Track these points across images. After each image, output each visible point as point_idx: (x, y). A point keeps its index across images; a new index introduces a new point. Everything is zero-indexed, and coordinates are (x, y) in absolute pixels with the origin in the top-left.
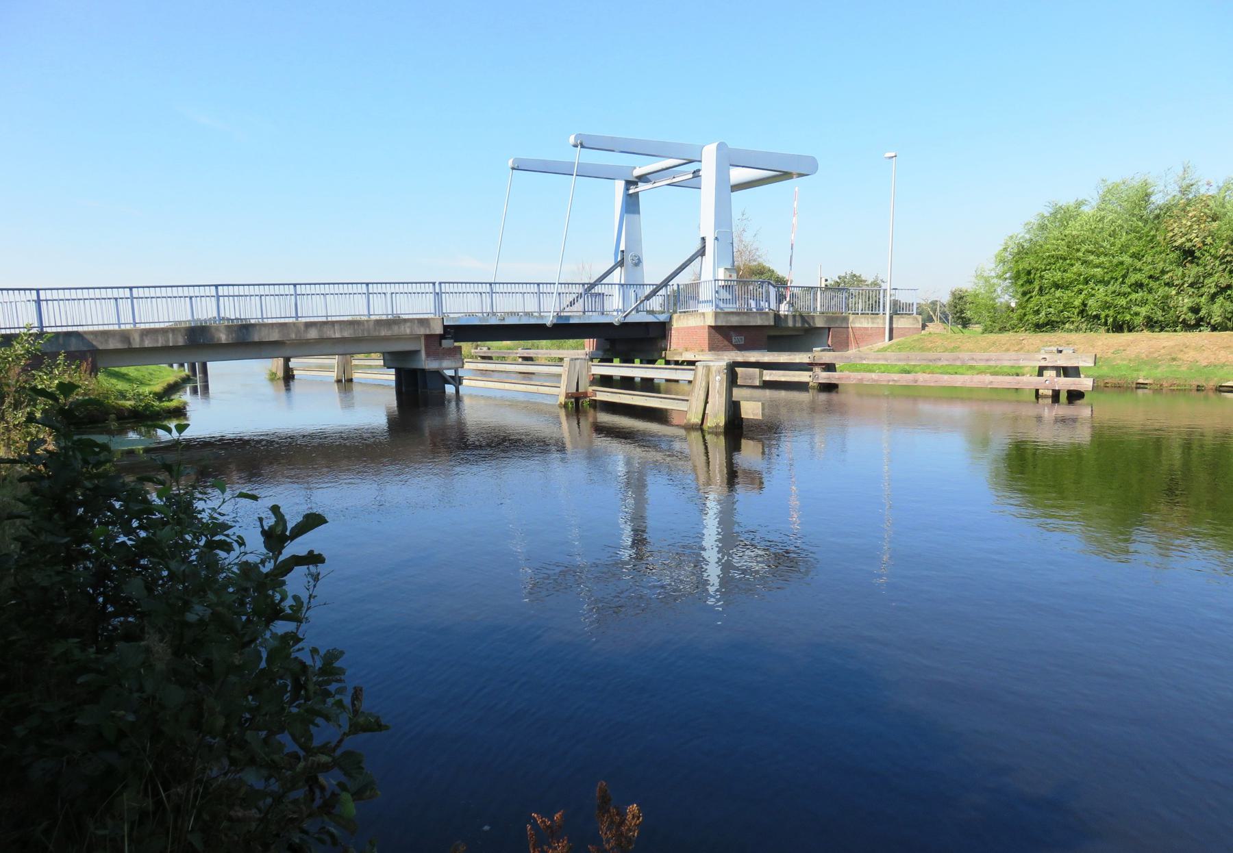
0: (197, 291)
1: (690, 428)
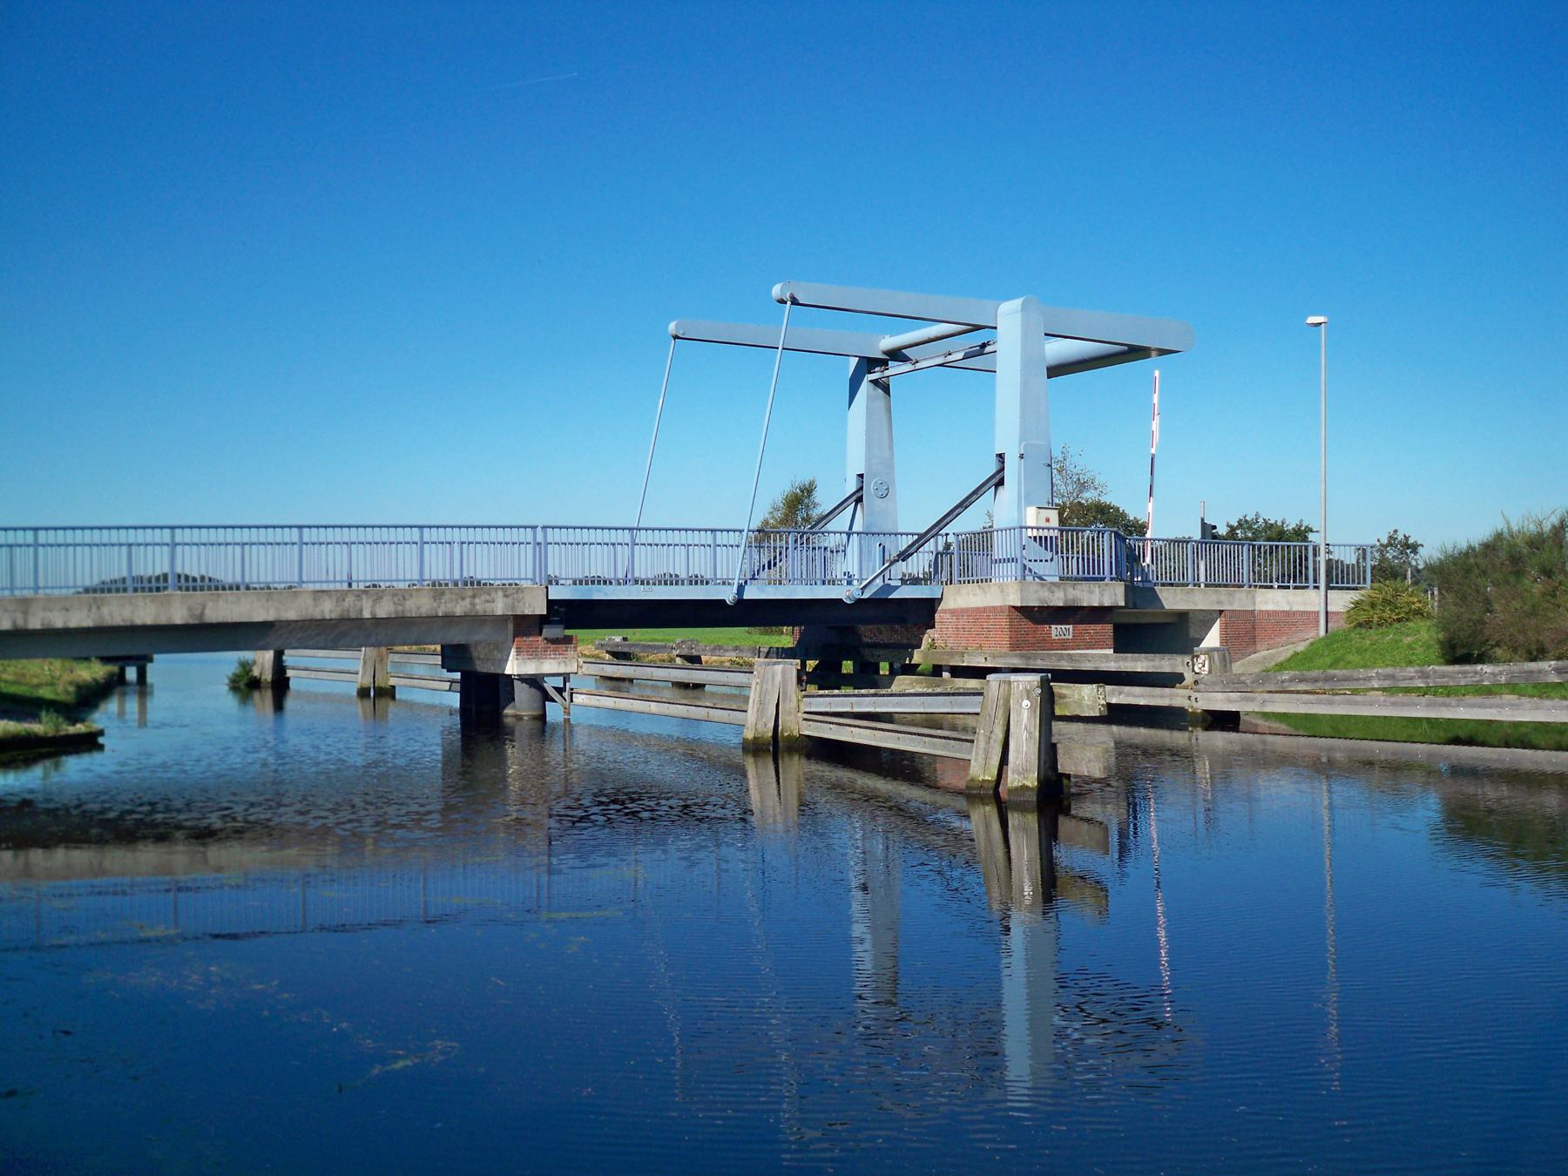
0: (140, 536)
1: (974, 794)
